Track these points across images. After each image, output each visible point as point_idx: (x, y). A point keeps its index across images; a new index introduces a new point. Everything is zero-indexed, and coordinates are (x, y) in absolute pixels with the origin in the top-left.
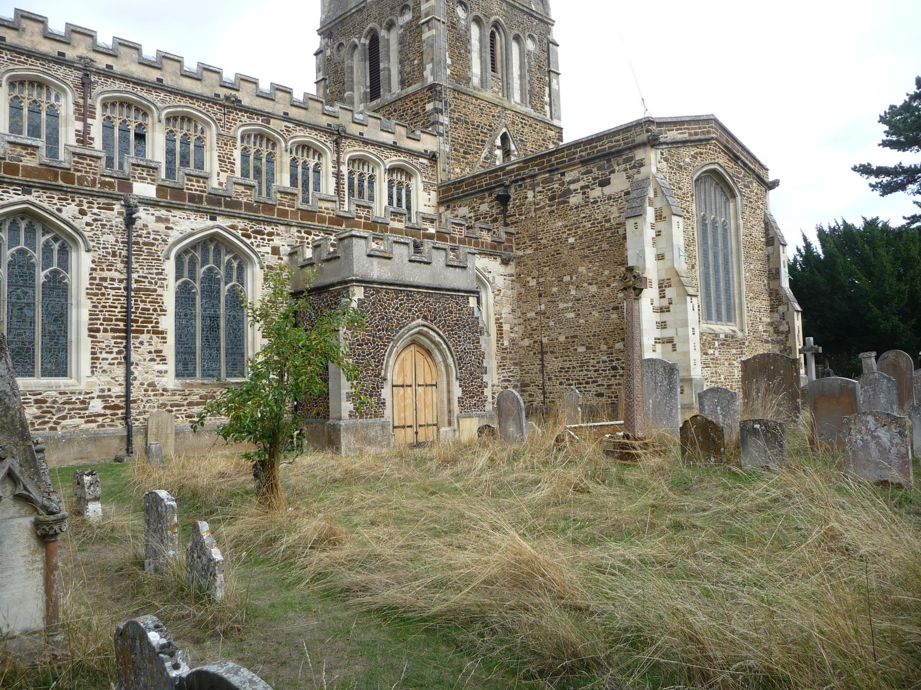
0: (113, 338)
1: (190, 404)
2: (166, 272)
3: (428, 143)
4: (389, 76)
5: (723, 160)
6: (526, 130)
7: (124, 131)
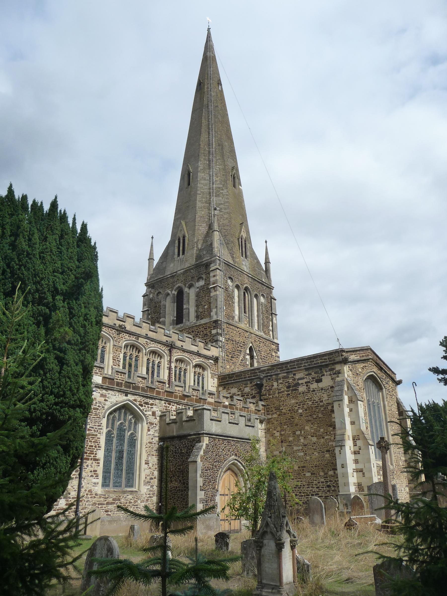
1: (108, 503)
2: (102, 425)
3: (214, 352)
5: (375, 369)
6: (261, 345)
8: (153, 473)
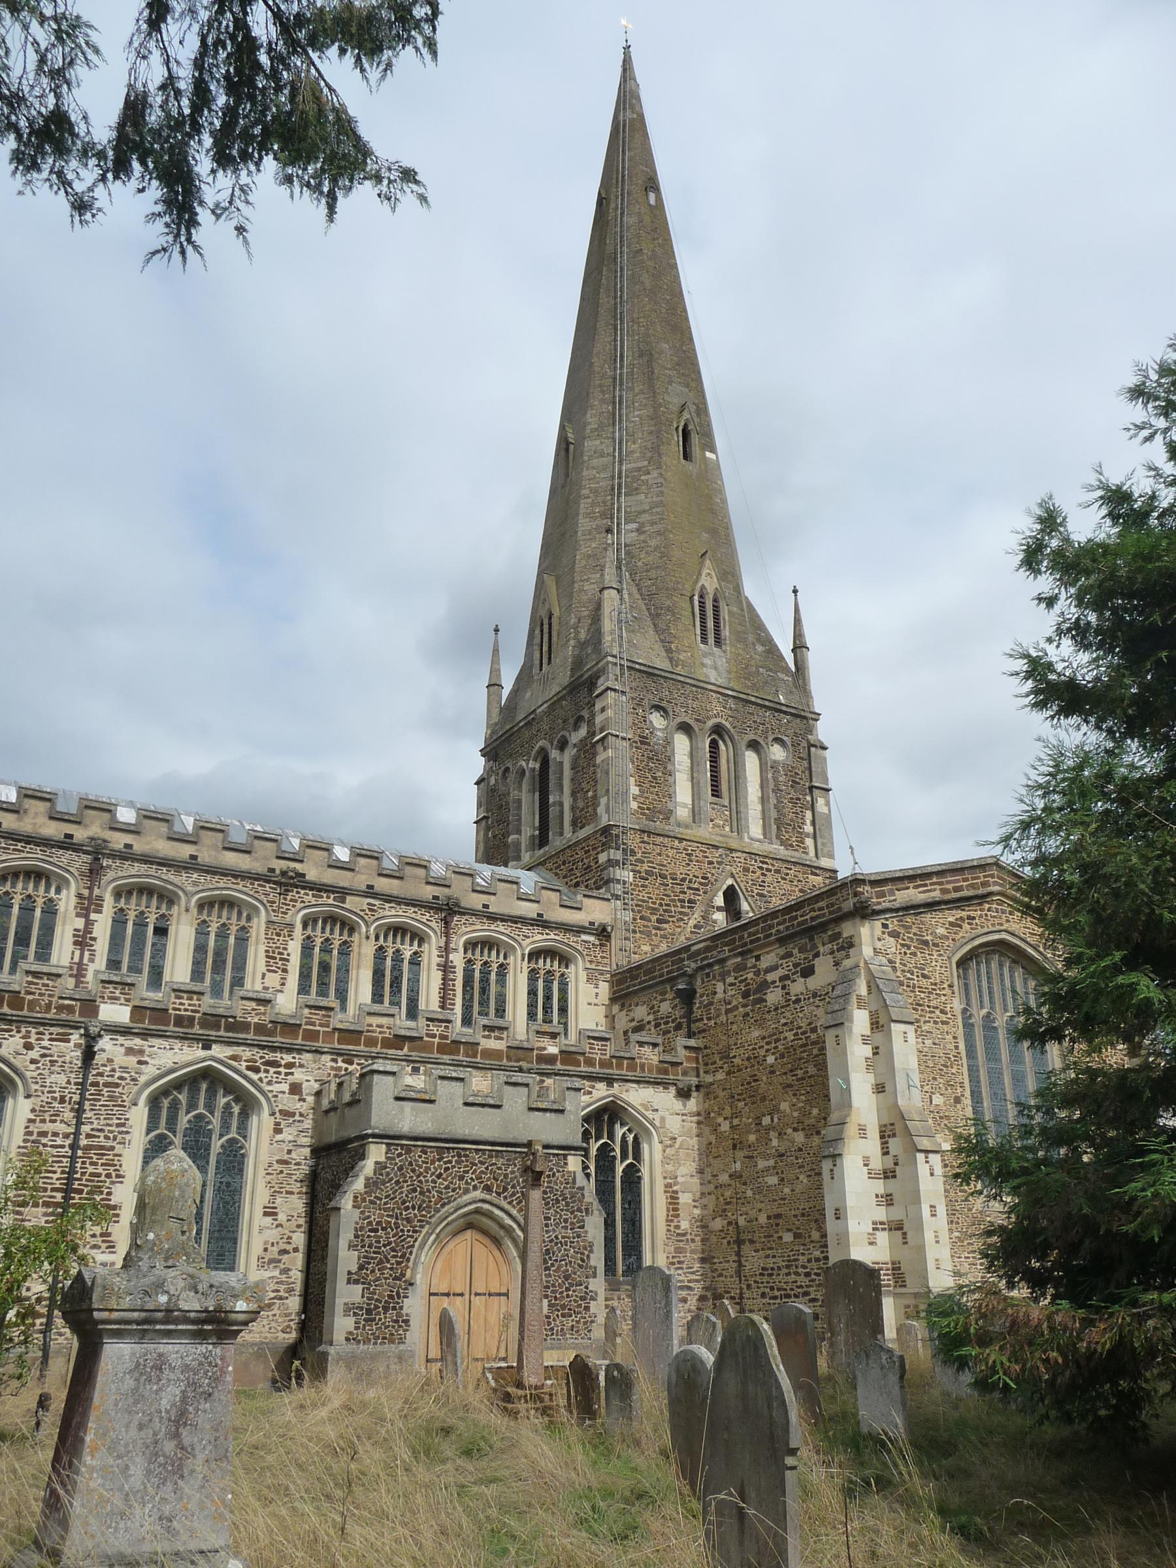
0: (45, 1214)
3: (595, 911)
4: (562, 812)
7: (141, 924)
8: (290, 1238)
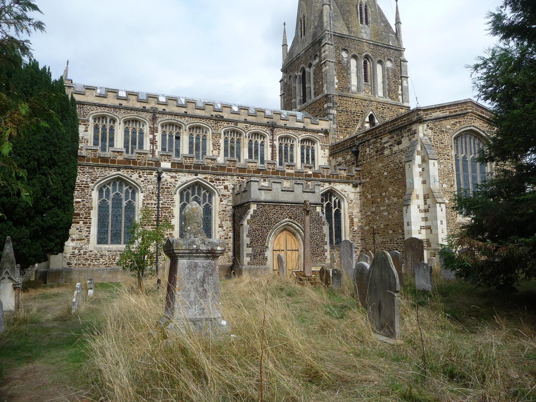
0: (152, 228)
3: (324, 125)
4: (310, 90)
7: (171, 136)
